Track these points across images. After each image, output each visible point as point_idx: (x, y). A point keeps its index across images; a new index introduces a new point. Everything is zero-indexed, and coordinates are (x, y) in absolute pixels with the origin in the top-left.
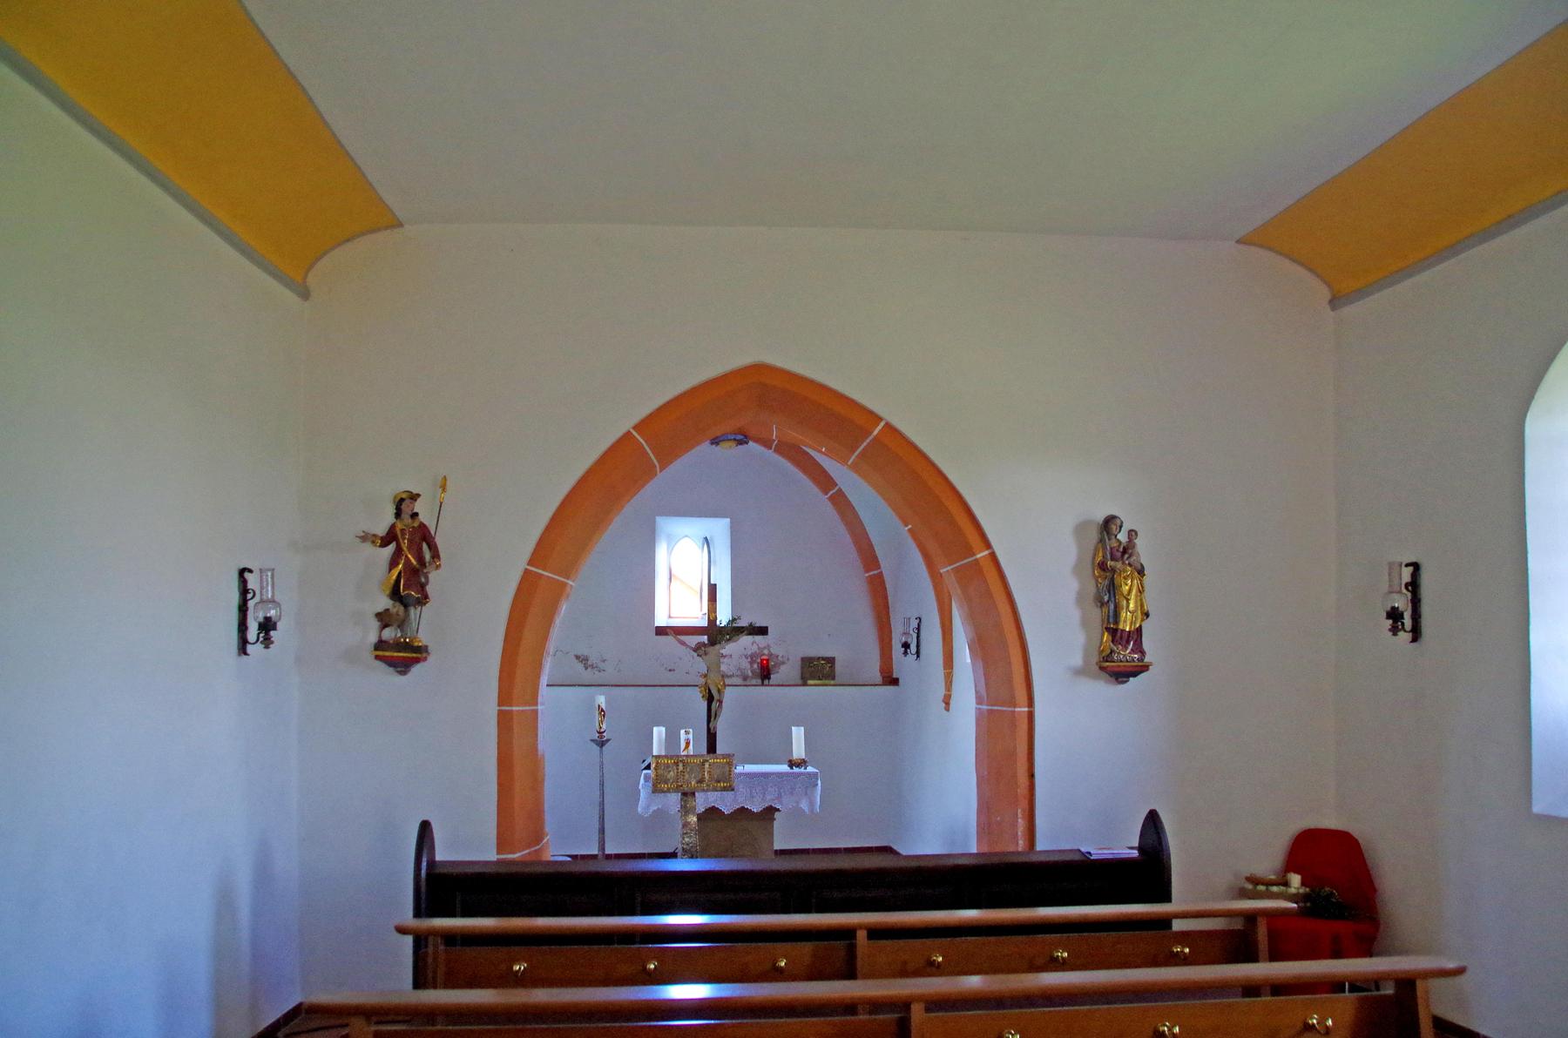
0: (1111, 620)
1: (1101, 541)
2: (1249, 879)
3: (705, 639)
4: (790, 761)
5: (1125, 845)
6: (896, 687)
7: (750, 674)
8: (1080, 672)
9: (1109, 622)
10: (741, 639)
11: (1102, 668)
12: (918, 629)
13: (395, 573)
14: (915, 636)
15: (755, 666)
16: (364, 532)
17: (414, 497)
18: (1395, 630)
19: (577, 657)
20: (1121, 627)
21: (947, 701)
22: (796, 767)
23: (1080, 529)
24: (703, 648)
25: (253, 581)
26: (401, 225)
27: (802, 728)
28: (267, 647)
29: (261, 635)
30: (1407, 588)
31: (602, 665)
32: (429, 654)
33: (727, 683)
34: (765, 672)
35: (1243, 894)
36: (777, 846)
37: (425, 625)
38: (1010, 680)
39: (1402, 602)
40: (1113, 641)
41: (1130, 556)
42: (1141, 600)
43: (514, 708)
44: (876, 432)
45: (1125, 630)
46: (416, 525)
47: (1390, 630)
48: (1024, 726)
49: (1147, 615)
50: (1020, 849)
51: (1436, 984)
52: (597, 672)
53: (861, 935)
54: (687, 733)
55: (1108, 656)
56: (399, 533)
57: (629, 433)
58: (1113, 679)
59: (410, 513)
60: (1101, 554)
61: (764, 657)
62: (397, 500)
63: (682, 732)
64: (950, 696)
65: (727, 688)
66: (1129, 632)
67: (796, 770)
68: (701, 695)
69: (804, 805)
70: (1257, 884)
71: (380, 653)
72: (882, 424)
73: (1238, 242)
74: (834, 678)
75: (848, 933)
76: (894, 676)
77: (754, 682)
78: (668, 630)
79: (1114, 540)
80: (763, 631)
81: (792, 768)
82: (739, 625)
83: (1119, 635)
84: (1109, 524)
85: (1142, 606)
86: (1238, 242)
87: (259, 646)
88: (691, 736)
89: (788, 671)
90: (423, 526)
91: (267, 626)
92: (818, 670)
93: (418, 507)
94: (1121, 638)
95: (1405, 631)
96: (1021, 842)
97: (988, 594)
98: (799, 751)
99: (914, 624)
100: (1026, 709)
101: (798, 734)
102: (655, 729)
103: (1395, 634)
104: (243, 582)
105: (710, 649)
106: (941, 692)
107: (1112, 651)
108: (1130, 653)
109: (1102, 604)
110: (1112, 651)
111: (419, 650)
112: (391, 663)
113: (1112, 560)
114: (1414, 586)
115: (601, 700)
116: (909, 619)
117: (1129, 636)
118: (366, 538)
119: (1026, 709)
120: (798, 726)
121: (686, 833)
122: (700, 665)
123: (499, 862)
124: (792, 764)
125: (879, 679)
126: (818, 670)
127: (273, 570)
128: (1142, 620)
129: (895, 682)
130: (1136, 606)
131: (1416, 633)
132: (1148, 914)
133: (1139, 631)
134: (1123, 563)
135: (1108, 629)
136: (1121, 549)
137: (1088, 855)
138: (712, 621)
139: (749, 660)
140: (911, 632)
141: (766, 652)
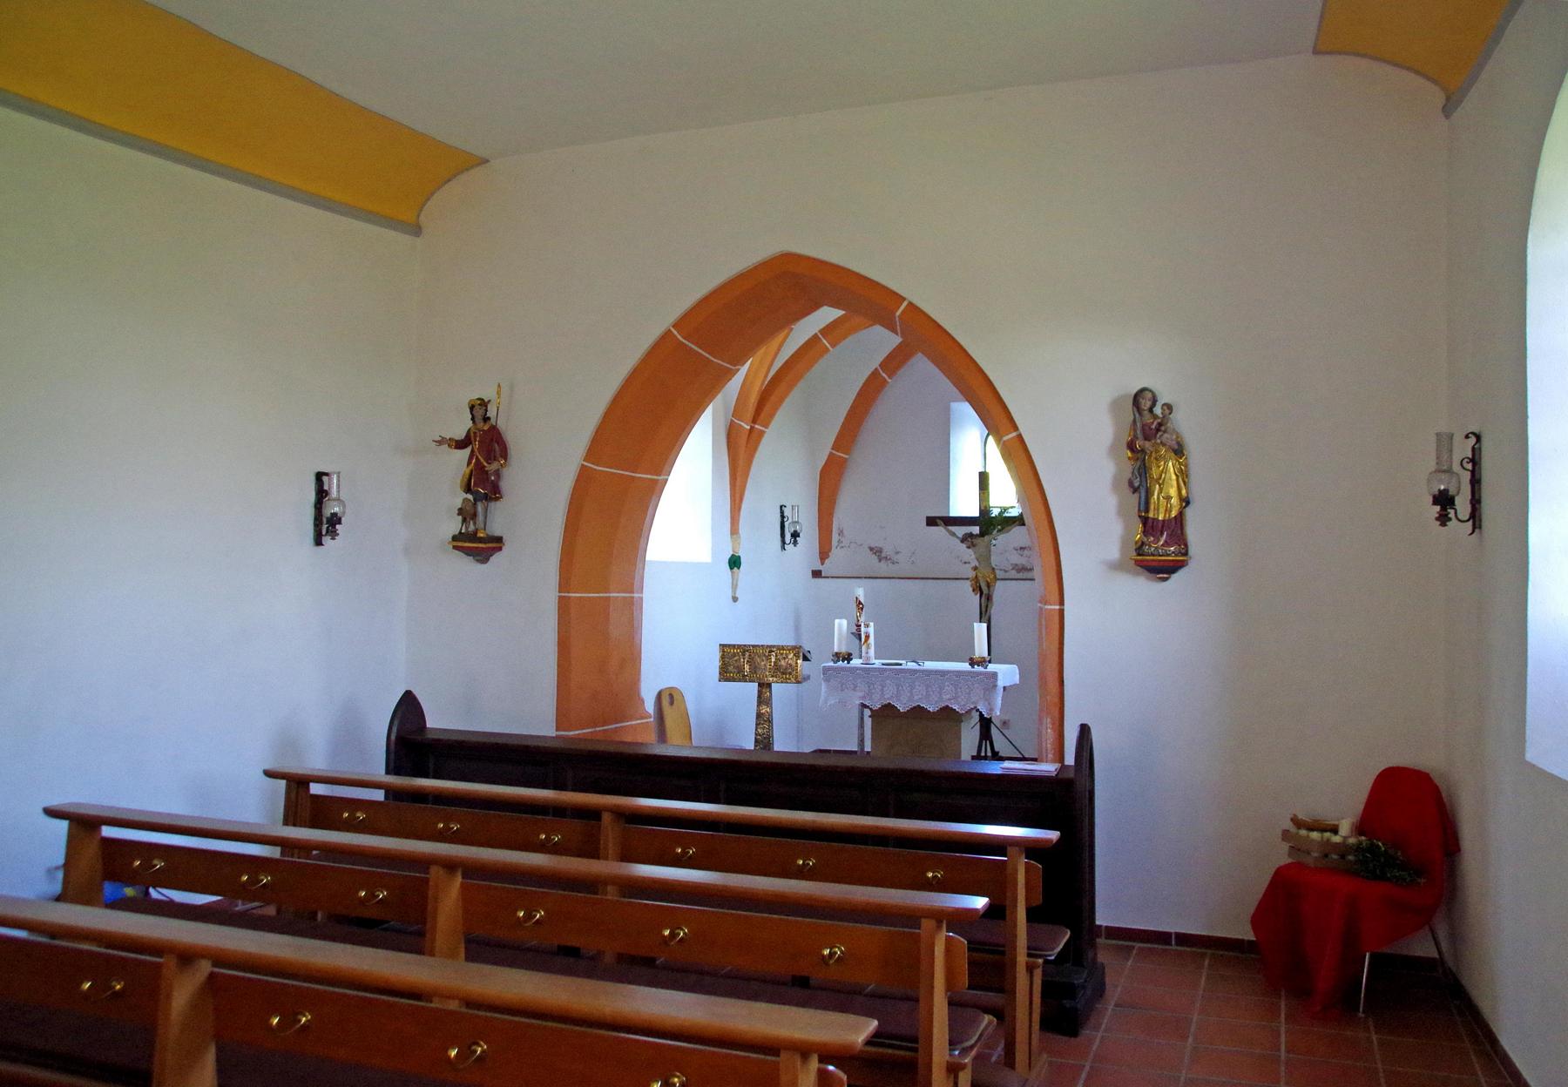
3: (976, 530)
4: (971, 659)
8: (1117, 567)
10: (1014, 530)
13: (470, 467)
19: (871, 549)
20: (1151, 515)
23: (1115, 405)
25: (787, 512)
26: (487, 161)
31: (895, 558)
33: (998, 577)
37: (498, 519)
43: (611, 595)
45: (1157, 520)
46: (486, 428)
47: (1437, 519)
52: (890, 564)
66: (1164, 521)
67: (977, 668)
70: (1299, 828)
71: (460, 544)
72: (905, 304)
75: (592, 814)
78: (938, 521)
87: (792, 545)
91: (795, 535)
98: (981, 649)
100: (1057, 607)
102: (837, 621)
103: (1443, 524)
105: (979, 541)
108: (1162, 545)
109: (1135, 490)
111: (499, 540)
112: (468, 552)
115: (860, 593)
117: (1163, 527)
122: (969, 555)
123: (557, 737)
124: (972, 663)
127: (339, 473)
132: (724, 814)
133: (1180, 518)
138: (985, 511)
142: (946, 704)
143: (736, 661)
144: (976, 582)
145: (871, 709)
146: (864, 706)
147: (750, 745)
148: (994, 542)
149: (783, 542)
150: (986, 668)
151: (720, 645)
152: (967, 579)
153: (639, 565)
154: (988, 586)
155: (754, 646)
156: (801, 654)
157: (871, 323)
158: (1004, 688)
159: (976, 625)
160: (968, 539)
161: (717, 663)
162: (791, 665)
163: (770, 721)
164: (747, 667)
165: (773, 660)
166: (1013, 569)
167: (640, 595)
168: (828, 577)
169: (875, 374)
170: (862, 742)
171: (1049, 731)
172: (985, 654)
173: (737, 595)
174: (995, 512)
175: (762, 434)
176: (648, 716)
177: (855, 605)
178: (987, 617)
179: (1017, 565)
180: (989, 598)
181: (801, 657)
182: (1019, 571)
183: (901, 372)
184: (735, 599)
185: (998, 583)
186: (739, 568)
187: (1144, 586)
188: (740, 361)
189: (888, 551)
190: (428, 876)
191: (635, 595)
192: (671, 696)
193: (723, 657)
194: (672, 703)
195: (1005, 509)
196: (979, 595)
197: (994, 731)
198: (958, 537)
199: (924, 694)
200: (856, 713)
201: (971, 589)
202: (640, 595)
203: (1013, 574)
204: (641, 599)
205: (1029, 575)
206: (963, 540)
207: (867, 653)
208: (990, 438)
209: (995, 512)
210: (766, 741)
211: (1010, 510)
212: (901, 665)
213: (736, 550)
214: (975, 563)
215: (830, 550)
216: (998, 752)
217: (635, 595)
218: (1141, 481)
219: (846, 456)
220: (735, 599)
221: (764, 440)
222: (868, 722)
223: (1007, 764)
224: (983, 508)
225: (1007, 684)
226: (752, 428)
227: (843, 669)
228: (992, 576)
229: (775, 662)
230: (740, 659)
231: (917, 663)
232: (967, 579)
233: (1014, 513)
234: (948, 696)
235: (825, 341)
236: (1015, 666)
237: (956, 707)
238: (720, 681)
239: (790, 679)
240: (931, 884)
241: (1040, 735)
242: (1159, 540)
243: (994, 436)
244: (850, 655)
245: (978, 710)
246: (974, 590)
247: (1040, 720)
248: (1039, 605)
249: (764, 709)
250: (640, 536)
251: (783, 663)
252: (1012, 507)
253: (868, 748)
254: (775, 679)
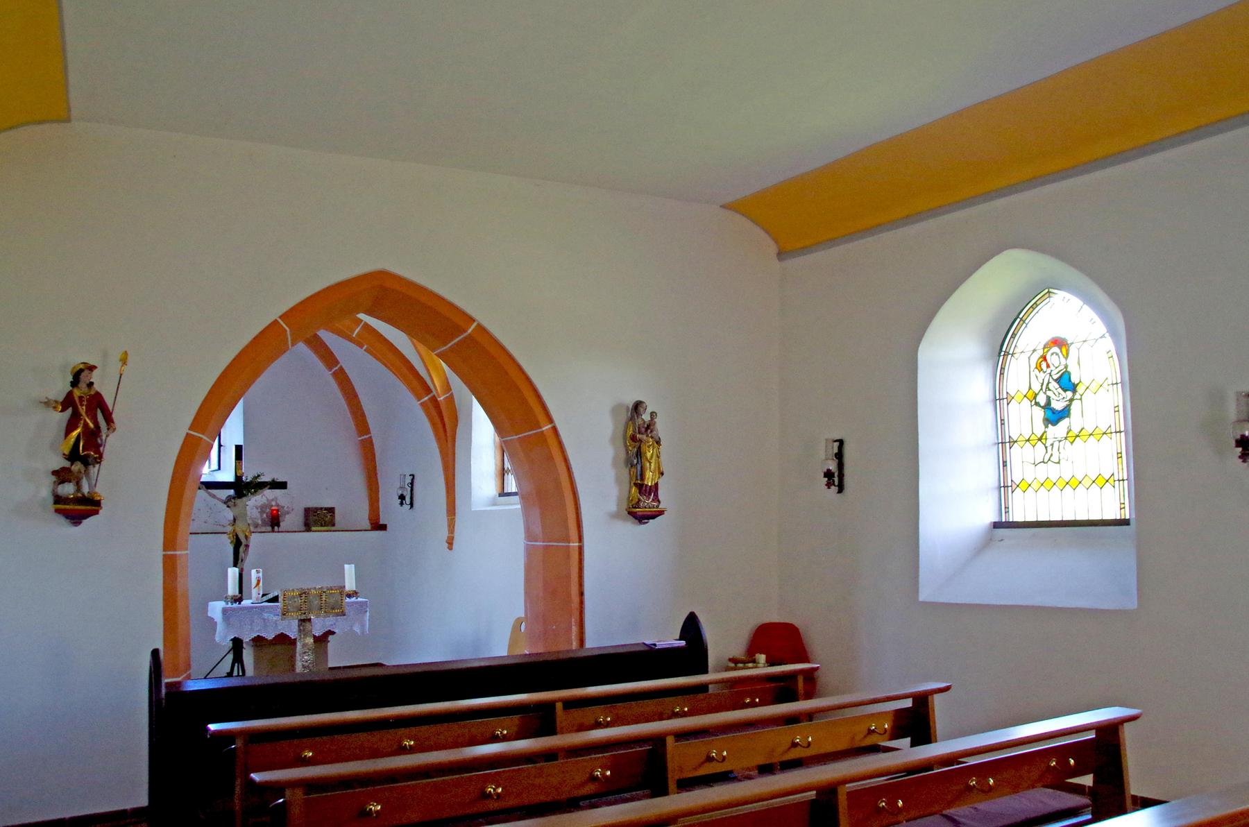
0: (639, 478)
1: (632, 419)
2: (731, 660)
3: (232, 492)
5: (670, 638)
6: (385, 532)
7: (260, 522)
8: (615, 516)
9: (637, 479)
11: (630, 513)
12: (412, 483)
14: (409, 489)
15: (265, 516)
16: (46, 398)
17: (92, 368)
18: (829, 485)
21: (450, 543)
23: (615, 410)
24: (233, 500)
27: (353, 565)
30: (836, 457)
32: (101, 508)
34: (274, 521)
35: (728, 669)
36: (331, 665)
38: (565, 521)
39: (833, 466)
40: (640, 493)
41: (651, 432)
42: (659, 463)
43: (541, 543)
44: (470, 331)
48: (575, 556)
49: (662, 474)
50: (574, 648)
51: (937, 697)
53: (559, 705)
54: (258, 572)
55: (636, 504)
56: (77, 399)
57: (276, 321)
58: (637, 521)
59: (88, 382)
60: (631, 429)
61: (273, 508)
62: (75, 370)
63: (254, 572)
64: (453, 538)
65: (253, 534)
66: (650, 486)
68: (230, 541)
69: (357, 629)
72: (475, 324)
73: (721, 206)
74: (334, 525)
76: (381, 523)
77: (263, 529)
79: (640, 420)
80: (282, 485)
82: (262, 480)
83: (644, 488)
84: (637, 407)
85: (659, 468)
86: (721, 206)
88: (261, 575)
89: (292, 519)
90: (98, 395)
92: (319, 518)
93: (95, 377)
94: (646, 490)
95: (835, 486)
96: (574, 643)
97: (550, 458)
99: (409, 480)
100: (577, 544)
101: (349, 570)
103: (829, 488)
106: (445, 534)
107: (639, 500)
110: (639, 500)
113: (639, 433)
114: (839, 456)
116: (405, 475)
118: (47, 403)
119: (577, 544)
120: (349, 564)
121: (305, 653)
122: (229, 515)
125: (367, 525)
126: (319, 518)
128: (659, 477)
129: (383, 527)
130: (655, 468)
131: (841, 489)
133: (656, 484)
134: (647, 436)
135: (635, 484)
136: (646, 426)
137: (653, 647)
139: (259, 510)
140: (407, 486)
141: (274, 503)
154: (246, 537)
160: (228, 502)
187: (631, 529)
218: (638, 461)
224: (238, 475)
240: (679, 714)
242: (649, 498)
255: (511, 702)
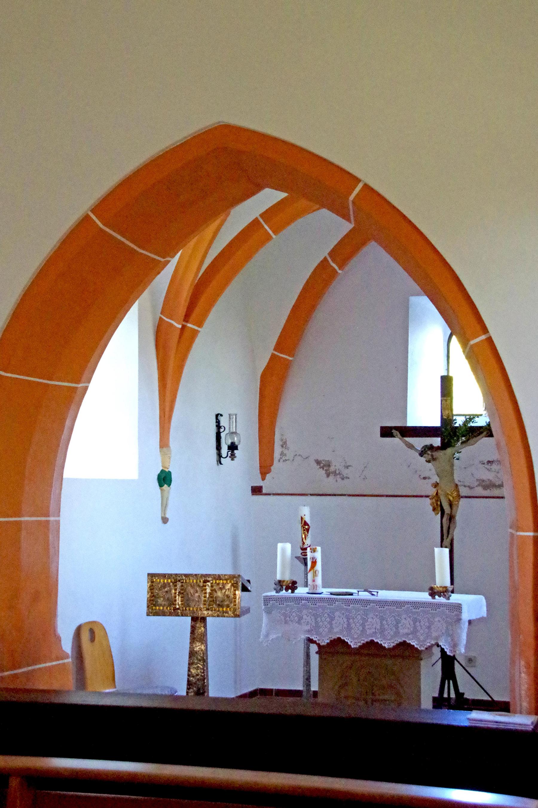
3: (437, 441)
4: (432, 589)
19: (318, 462)
22: (440, 596)
25: (224, 422)
28: (232, 460)
29: (229, 453)
31: (345, 472)
43: (22, 519)
52: (339, 480)
78: (394, 431)
81: (433, 598)
87: (228, 459)
91: (233, 447)
100: (531, 534)
102: (280, 545)
104: (218, 422)
105: (440, 454)
115: (306, 513)
119: (531, 534)
122: (429, 469)
124: (433, 593)
142: (404, 639)
143: (167, 592)
144: (437, 501)
145: (318, 645)
146: (311, 641)
147: (182, 691)
148: (457, 455)
149: (220, 455)
150: (448, 599)
151: (149, 574)
152: (427, 496)
153: (55, 484)
155: (186, 575)
156: (240, 584)
157: (318, 206)
158: (470, 622)
159: (437, 550)
161: (144, 595)
162: (228, 597)
163: (204, 660)
164: (179, 600)
165: (208, 591)
166: (479, 485)
167: (57, 519)
168: (269, 494)
169: (324, 264)
170: (308, 680)
171: (523, 675)
172: (448, 583)
173: (167, 516)
174: (459, 421)
175: (195, 333)
176: (67, 656)
177: (300, 526)
178: (449, 540)
179: (483, 481)
180: (451, 518)
181: (240, 588)
182: (485, 488)
183: (353, 262)
184: (165, 520)
185: (462, 501)
186: (169, 485)
188: (169, 252)
189: (336, 465)
190: (199, 329)
191: (52, 519)
192: (92, 632)
193: (151, 588)
194: (92, 639)
195: (471, 418)
196: (439, 515)
197: (458, 669)
198: (416, 450)
199: (378, 627)
200: (301, 647)
201: (431, 508)
202: (57, 519)
203: (480, 491)
204: (58, 522)
205: (496, 492)
206: (422, 454)
207: (314, 581)
208: (454, 338)
209: (459, 421)
210: (200, 684)
211: (476, 419)
212: (351, 594)
213: (167, 466)
214: (435, 479)
215: (272, 464)
216: (463, 694)
217: (52, 519)
219: (291, 359)
220: (165, 520)
221: (198, 342)
222: (315, 659)
223: (476, 715)
224: (445, 417)
225: (473, 617)
226: (184, 327)
227: (287, 599)
228: (455, 494)
229: (210, 594)
230: (170, 591)
231: (370, 592)
232: (427, 496)
233: (481, 422)
234: (406, 631)
235: (266, 227)
236: (482, 596)
237: (413, 643)
238: (148, 615)
239: (227, 612)
241: (512, 681)
243: (456, 336)
244: (294, 583)
245: (438, 646)
246: (434, 510)
247: (513, 662)
248: (510, 530)
249: (199, 647)
250: (56, 452)
251: (219, 594)
252: (478, 416)
253: (315, 687)
254: (210, 612)
255: (317, 790)
